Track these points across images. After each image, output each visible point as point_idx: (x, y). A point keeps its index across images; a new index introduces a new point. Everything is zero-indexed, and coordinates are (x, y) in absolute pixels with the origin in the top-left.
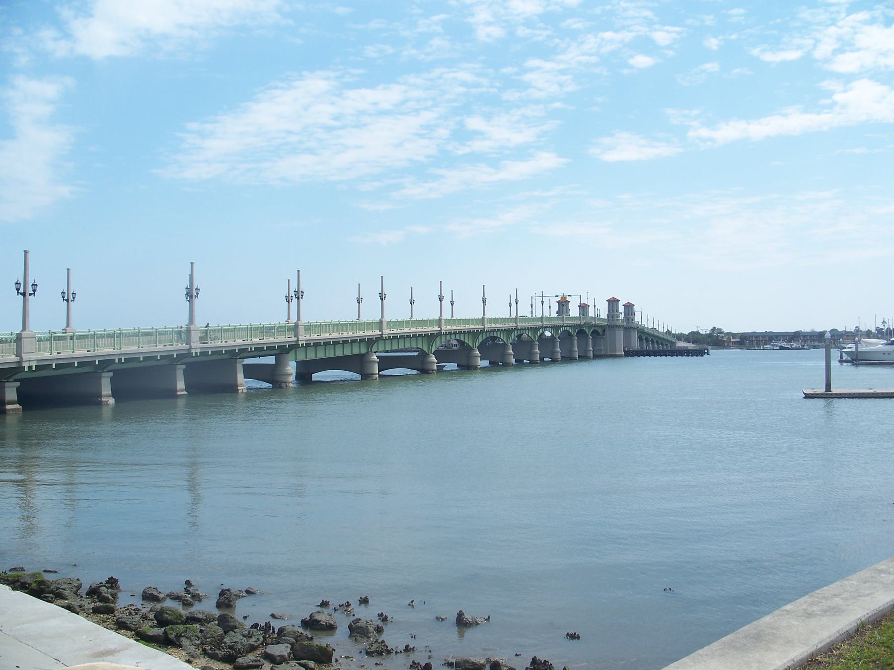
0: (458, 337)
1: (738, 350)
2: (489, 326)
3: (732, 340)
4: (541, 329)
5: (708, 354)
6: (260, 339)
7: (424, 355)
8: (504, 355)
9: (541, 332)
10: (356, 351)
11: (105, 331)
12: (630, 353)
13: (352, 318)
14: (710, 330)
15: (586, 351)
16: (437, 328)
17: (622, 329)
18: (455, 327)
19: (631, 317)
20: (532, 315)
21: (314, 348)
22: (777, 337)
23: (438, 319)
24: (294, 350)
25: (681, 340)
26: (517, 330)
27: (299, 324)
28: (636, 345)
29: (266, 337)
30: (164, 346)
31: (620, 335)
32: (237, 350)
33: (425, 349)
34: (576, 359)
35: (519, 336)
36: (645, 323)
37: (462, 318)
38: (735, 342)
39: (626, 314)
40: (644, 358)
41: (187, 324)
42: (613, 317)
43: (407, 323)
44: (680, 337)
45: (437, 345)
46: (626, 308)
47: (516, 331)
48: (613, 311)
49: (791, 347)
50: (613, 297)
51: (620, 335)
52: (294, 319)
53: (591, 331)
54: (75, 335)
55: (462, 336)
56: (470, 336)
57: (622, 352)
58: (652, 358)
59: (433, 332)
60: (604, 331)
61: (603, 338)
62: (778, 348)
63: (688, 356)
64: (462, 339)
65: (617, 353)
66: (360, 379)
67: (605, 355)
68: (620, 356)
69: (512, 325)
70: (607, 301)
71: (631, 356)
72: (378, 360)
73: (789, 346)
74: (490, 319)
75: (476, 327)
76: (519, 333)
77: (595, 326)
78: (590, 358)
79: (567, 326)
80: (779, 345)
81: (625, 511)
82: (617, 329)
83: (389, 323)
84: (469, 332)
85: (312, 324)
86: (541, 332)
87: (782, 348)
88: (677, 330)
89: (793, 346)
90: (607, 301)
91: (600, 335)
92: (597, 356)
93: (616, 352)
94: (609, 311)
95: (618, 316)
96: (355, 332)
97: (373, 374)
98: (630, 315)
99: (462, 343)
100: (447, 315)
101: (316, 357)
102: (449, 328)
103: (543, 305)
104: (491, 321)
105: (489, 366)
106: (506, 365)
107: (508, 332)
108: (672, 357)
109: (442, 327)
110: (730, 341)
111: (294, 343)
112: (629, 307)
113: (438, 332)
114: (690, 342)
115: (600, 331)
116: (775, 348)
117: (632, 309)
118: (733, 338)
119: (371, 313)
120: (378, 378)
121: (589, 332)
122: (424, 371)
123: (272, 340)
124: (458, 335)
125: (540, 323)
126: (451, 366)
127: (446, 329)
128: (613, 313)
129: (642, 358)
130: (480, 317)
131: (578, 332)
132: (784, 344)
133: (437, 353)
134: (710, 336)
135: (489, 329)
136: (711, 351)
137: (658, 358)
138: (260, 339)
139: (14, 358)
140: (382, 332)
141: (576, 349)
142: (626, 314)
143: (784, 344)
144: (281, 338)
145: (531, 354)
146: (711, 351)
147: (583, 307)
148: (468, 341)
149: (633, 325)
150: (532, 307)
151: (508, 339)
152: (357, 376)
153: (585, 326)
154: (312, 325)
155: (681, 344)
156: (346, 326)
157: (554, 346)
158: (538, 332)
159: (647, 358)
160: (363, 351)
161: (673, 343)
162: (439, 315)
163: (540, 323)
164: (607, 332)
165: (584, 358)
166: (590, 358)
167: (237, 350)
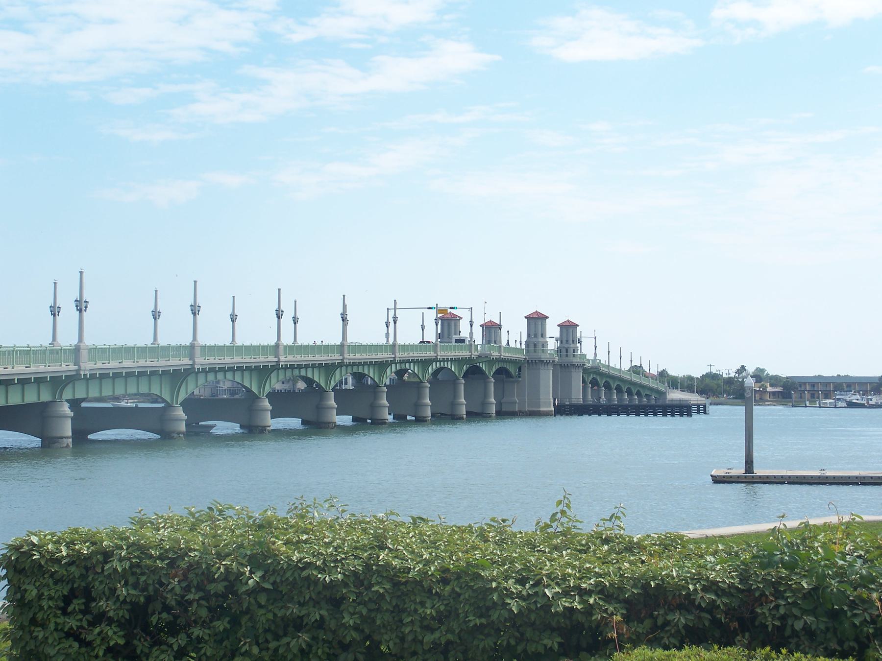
0: (303, 373)
1: (781, 407)
2: (352, 356)
3: (769, 389)
4: (434, 363)
5: (705, 413)
6: (26, 367)
7: (252, 398)
8: (374, 407)
9: (434, 367)
10: (31, 397)
11: (41, 347)
12: (563, 410)
13: (145, 339)
14: (735, 370)
15: (485, 403)
16: (187, 361)
17: (551, 367)
18: (507, 354)
19: (572, 345)
20: (388, 341)
21: (35, 385)
22: (849, 385)
23: (339, 344)
24: (70, 385)
25: (677, 389)
26: (396, 364)
27: (82, 347)
28: (577, 395)
29: (125, 359)
30: (4, 368)
31: (547, 377)
32: (16, 380)
33: (255, 389)
34: (462, 418)
35: (400, 373)
36: (603, 358)
37: (406, 344)
38: (774, 393)
39: (564, 342)
40: (599, 417)
41: (50, 342)
42: (535, 346)
43: (143, 351)
44: (675, 383)
45: (275, 384)
46: (565, 330)
47: (393, 365)
48: (536, 336)
49: (868, 403)
50: (537, 312)
51: (547, 377)
52: (391, 341)
53: (494, 370)
54: (32, 349)
55: (310, 371)
56: (375, 368)
57: (550, 407)
58: (604, 418)
59: (223, 366)
60: (520, 370)
61: (518, 382)
62: (844, 404)
63: (673, 415)
64: (310, 375)
65: (542, 409)
66: (40, 446)
67: (520, 412)
68: (547, 414)
69: (386, 356)
70: (525, 317)
71: (567, 415)
72: (72, 414)
73: (864, 402)
74: (402, 345)
75: (331, 358)
76: (398, 368)
77: (499, 360)
78: (490, 417)
79: (444, 360)
80: (848, 399)
81: (880, 454)
82: (573, 370)
83: (203, 348)
84: (165, 373)
85: (98, 347)
86: (434, 367)
87: (851, 405)
88: (677, 371)
89: (871, 402)
90: (525, 317)
91: (512, 377)
92: (503, 414)
93: (539, 407)
94: (529, 336)
95: (544, 344)
96: (107, 362)
97: (62, 438)
98: (571, 342)
99: (309, 381)
100: (287, 339)
101: (7, 403)
102: (290, 358)
103: (471, 326)
104: (97, 352)
105: (352, 423)
106: (378, 424)
107: (382, 366)
108: (637, 417)
109: (502, 353)
110: (765, 391)
111: (74, 373)
112: (568, 329)
113: (340, 361)
114: (693, 392)
115: (512, 369)
116: (840, 404)
117: (574, 332)
118: (771, 385)
119: (67, 339)
120: (71, 446)
121: (489, 372)
122: (167, 436)
123: (42, 368)
124: (290, 370)
125: (468, 353)
126: (223, 427)
127: (349, 357)
128: (535, 340)
129: (586, 417)
130: (338, 343)
131: (467, 371)
132: (856, 398)
133: (273, 396)
134: (730, 381)
135: (401, 359)
136: (711, 409)
137: (614, 418)
138: (26, 367)
139: (73, 367)
140: (79, 366)
141: (463, 400)
142: (564, 342)
143: (856, 398)
144: (55, 366)
145: (418, 406)
146: (711, 407)
147: (491, 329)
148: (317, 377)
149: (576, 361)
150: (388, 327)
151: (381, 377)
152: (36, 442)
153: (481, 360)
154: (17, 351)
155: (676, 395)
156: (28, 354)
157: (420, 396)
158: (430, 368)
159: (595, 418)
160: (46, 397)
161: (662, 394)
162: (341, 340)
163: (433, 354)
164: (525, 371)
165: (477, 415)
166: (490, 417)
167: (16, 380)
